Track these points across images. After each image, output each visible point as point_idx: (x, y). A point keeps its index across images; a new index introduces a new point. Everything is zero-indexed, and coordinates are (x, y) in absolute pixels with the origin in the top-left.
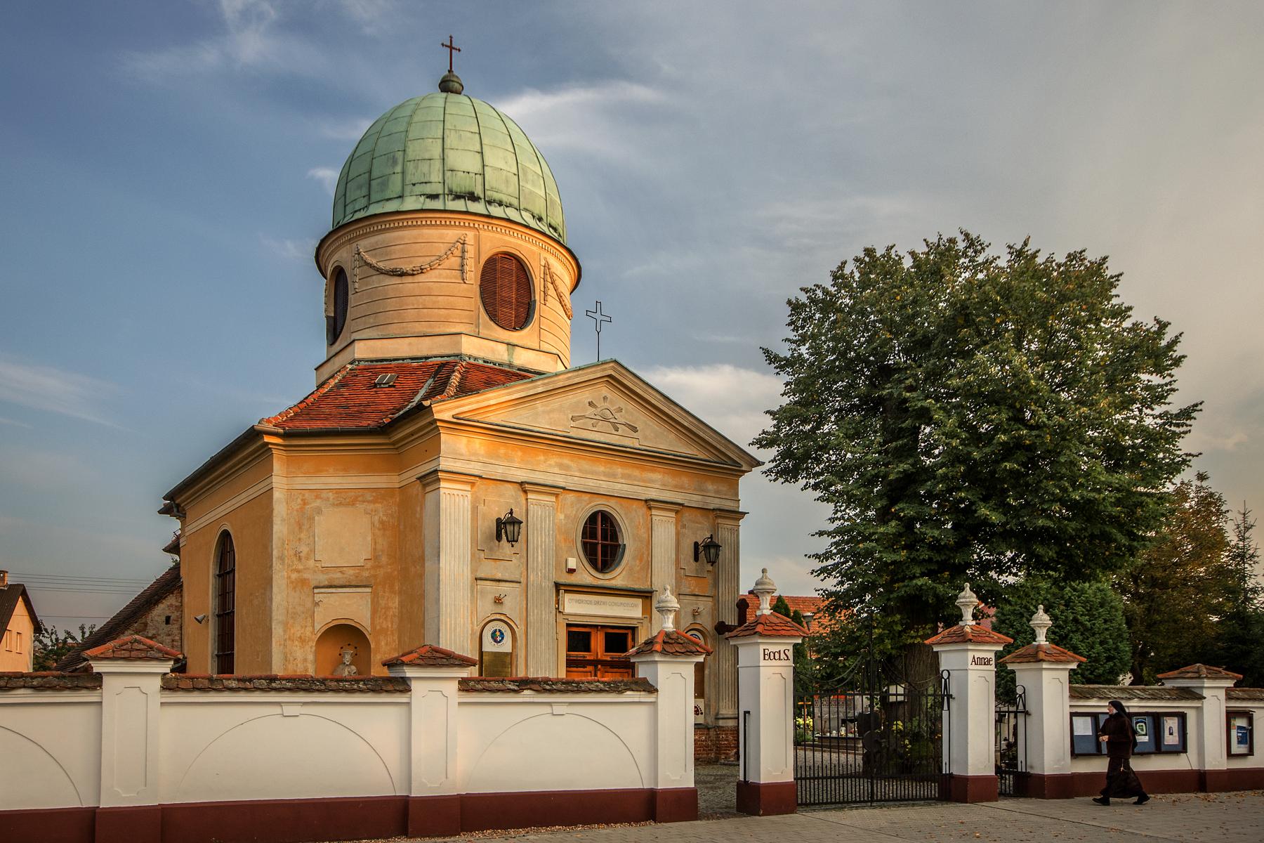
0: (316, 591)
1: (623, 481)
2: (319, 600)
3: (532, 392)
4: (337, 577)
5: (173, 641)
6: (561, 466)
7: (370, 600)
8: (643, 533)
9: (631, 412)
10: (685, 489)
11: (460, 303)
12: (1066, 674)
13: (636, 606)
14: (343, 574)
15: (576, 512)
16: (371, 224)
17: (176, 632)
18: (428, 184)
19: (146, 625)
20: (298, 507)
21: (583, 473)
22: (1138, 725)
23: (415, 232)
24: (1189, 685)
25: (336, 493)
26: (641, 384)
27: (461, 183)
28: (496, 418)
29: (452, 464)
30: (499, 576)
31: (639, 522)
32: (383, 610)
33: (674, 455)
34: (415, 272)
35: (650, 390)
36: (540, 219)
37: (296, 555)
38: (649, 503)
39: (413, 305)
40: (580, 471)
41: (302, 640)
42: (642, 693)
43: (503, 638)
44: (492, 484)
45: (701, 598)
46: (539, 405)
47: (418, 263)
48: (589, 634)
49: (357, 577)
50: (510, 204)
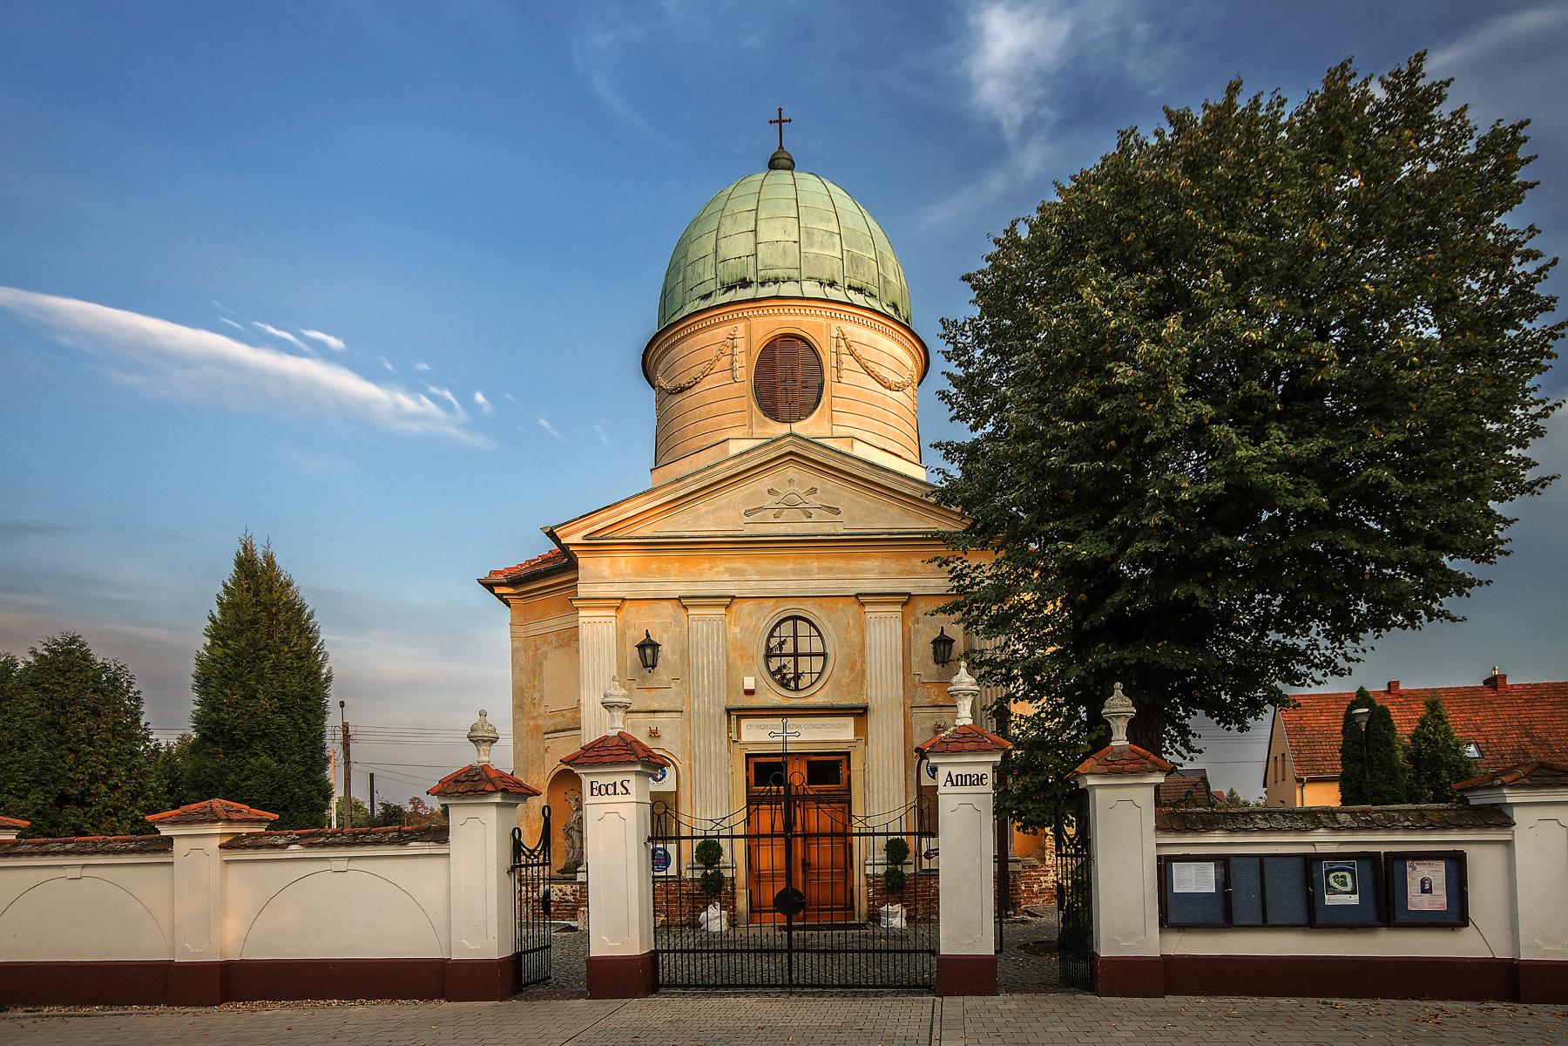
0: (546, 736)
1: (821, 576)
3: (682, 493)
6: (732, 571)
8: (854, 636)
9: (831, 489)
10: (918, 573)
11: (733, 405)
12: (1151, 792)
13: (845, 726)
15: (756, 622)
21: (764, 575)
22: (1332, 876)
24: (1488, 801)
26: (833, 454)
27: (732, 272)
28: (646, 530)
29: (592, 590)
30: (655, 706)
31: (849, 624)
33: (889, 534)
35: (848, 460)
36: (832, 284)
38: (861, 599)
39: (691, 420)
40: (759, 573)
42: (431, 844)
43: (664, 776)
44: (644, 606)
45: (945, 710)
46: (702, 506)
47: (695, 372)
48: (786, 763)
50: (788, 278)
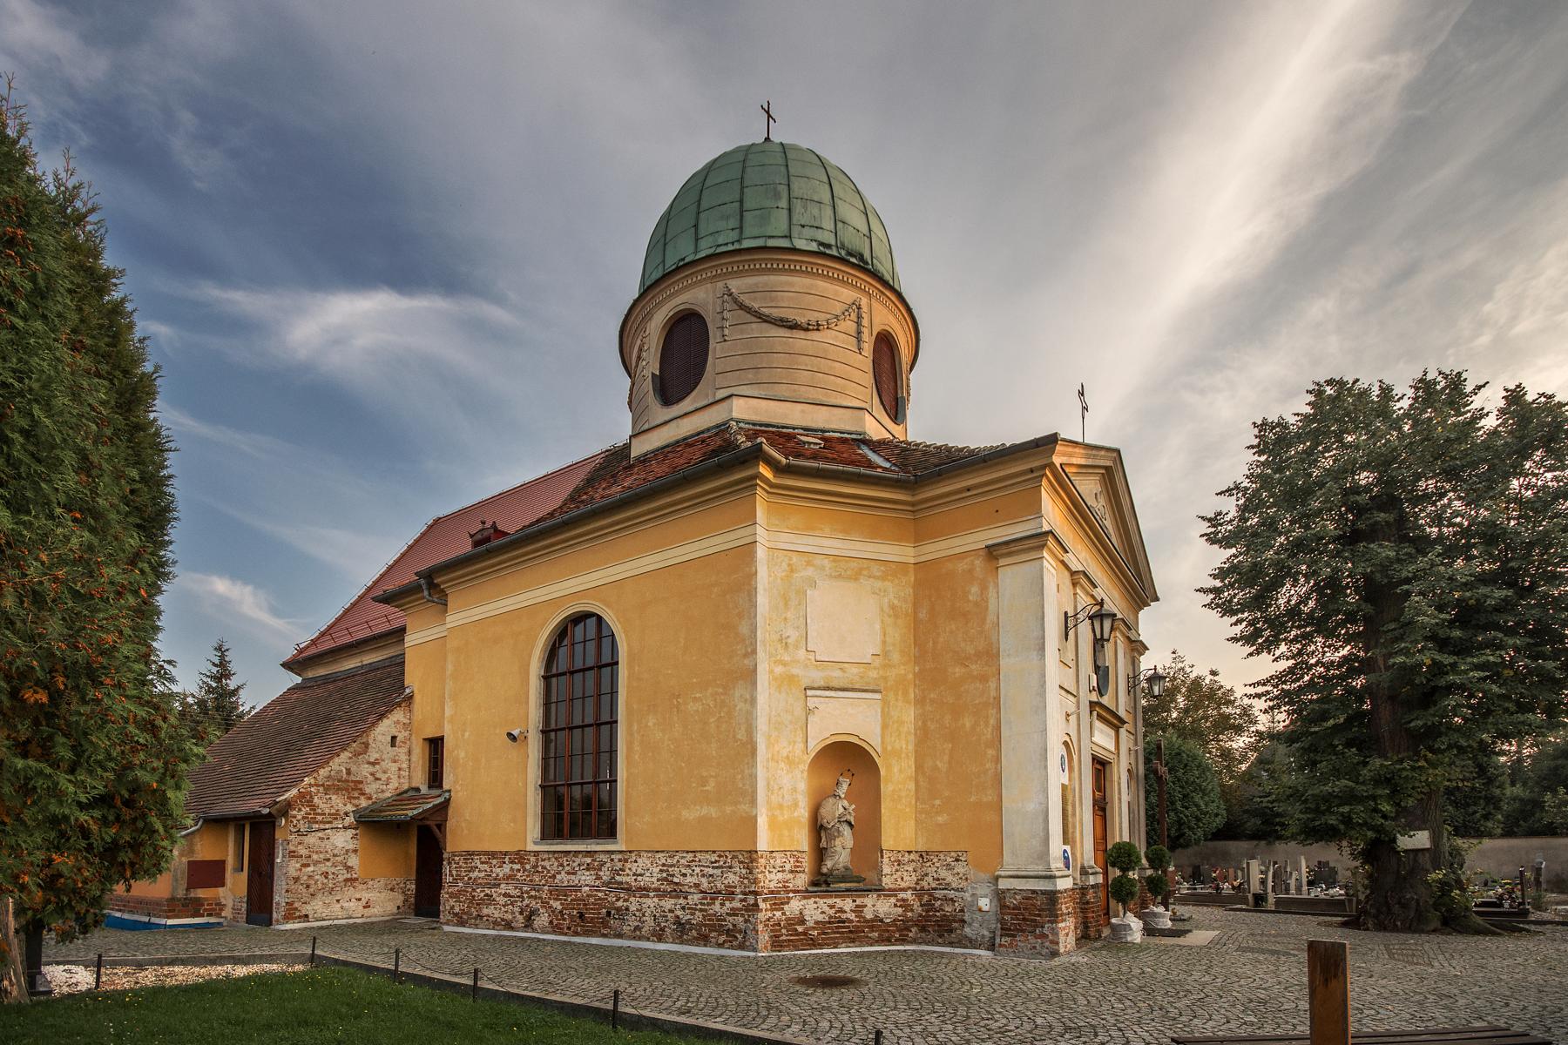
0: (809, 693)
2: (814, 705)
4: (837, 677)
5: (400, 769)
7: (879, 711)
11: (857, 376)
14: (844, 672)
16: (753, 260)
17: (404, 757)
18: (820, 231)
19: (367, 745)
20: (783, 574)
23: (807, 281)
25: (834, 561)
32: (895, 725)
34: (811, 327)
37: (781, 640)
41: (790, 761)
47: (813, 317)
49: (862, 677)
